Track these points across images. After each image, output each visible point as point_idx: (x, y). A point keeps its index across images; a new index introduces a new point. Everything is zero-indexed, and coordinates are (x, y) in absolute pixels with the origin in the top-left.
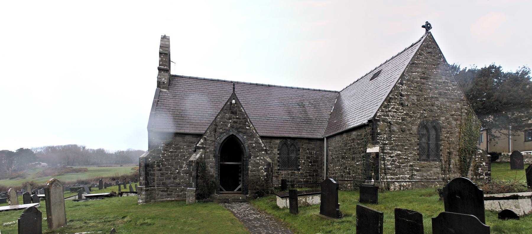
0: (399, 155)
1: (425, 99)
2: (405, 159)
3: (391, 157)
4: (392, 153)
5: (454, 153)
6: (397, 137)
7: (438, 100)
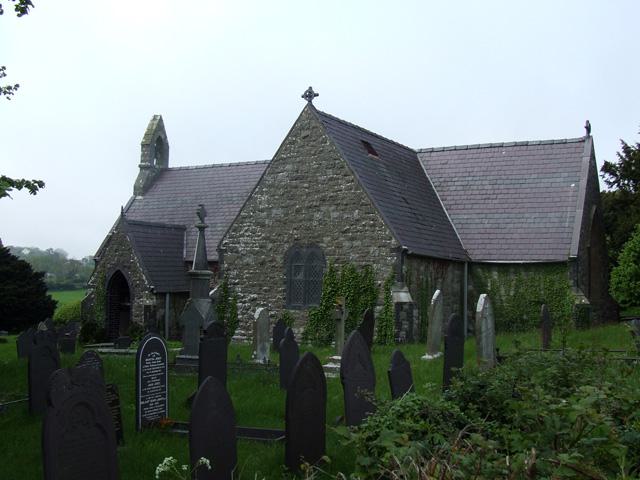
0: (254, 300)
1: (298, 211)
3: (245, 302)
7: (319, 211)
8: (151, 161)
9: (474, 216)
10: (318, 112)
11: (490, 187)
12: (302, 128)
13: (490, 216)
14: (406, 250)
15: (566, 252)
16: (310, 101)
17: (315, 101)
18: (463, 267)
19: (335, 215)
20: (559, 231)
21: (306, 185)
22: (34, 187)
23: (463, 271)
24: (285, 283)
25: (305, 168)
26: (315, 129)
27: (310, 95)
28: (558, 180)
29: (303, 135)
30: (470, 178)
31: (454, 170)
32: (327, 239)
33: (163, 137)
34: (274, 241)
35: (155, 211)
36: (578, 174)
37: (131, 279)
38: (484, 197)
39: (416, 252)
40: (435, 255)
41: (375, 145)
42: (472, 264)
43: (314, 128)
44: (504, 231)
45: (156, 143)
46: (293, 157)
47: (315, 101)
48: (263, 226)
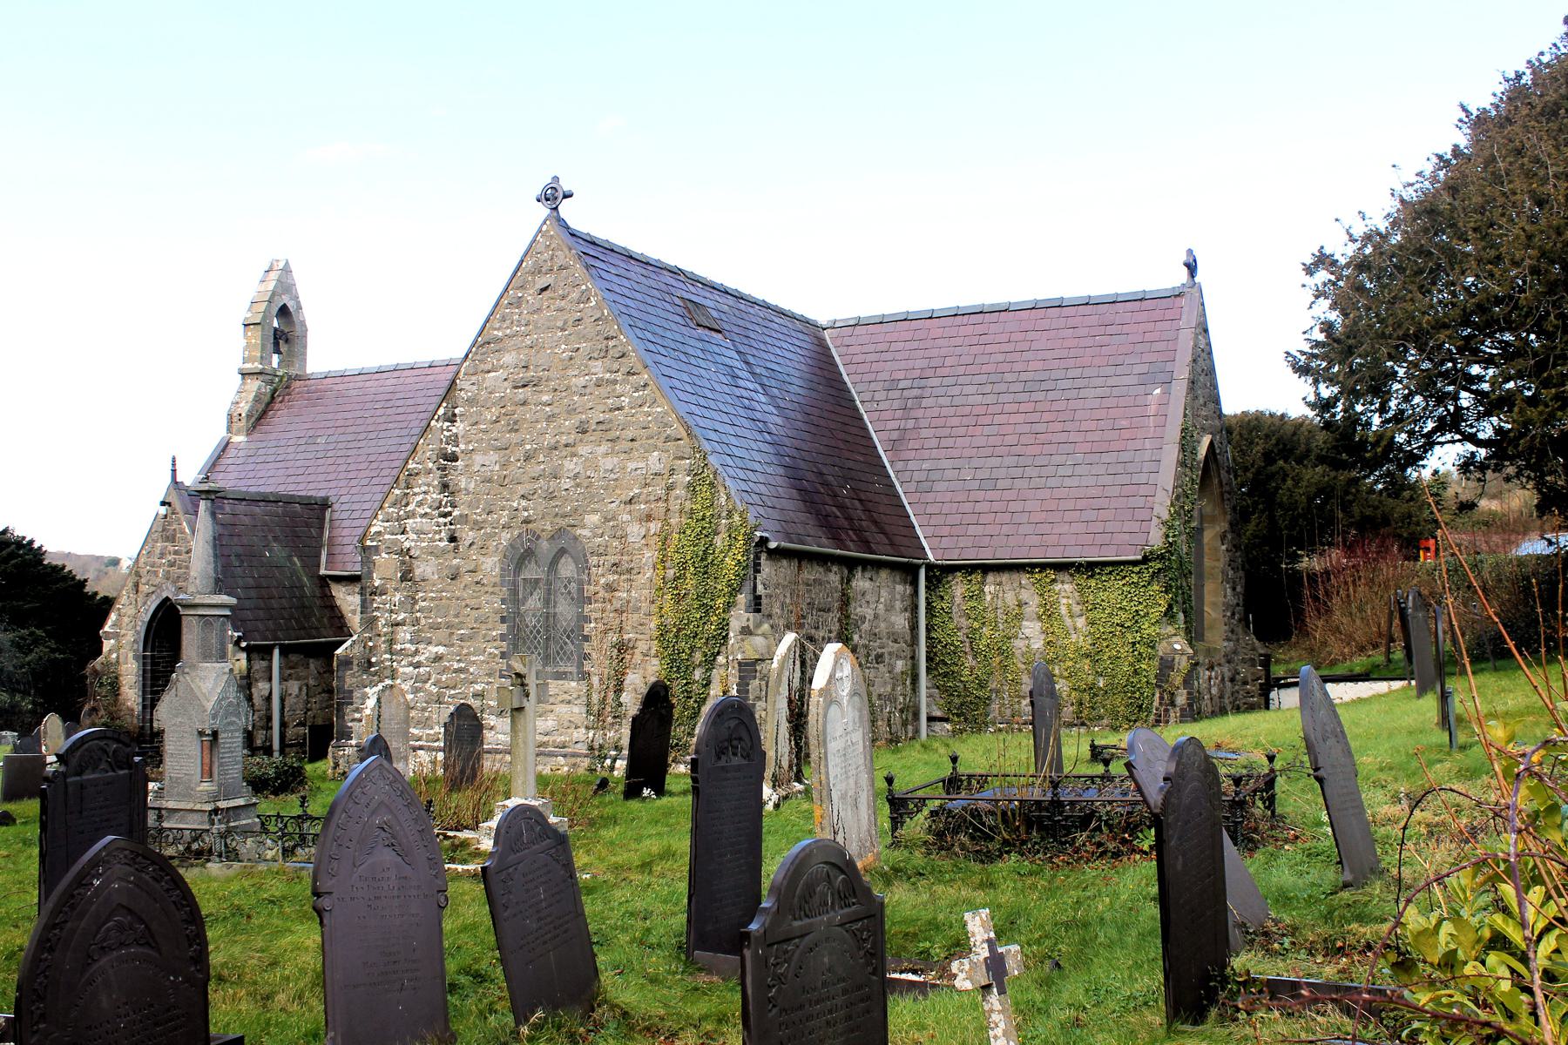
0: (438, 658)
1: (528, 457)
2: (460, 670)
3: (417, 665)
4: (417, 652)
5: (642, 646)
6: (432, 599)
7: (574, 455)
12: (538, 271)
15: (1140, 539)
17: (565, 209)
18: (271, 654)
19: (609, 463)
21: (545, 398)
24: (503, 620)
25: (542, 359)
26: (592, 279)
27: (553, 196)
29: (540, 286)
31: (903, 365)
33: (291, 305)
34: (477, 526)
35: (279, 473)
36: (1169, 367)
43: (561, 268)
44: (1007, 495)
45: (281, 328)
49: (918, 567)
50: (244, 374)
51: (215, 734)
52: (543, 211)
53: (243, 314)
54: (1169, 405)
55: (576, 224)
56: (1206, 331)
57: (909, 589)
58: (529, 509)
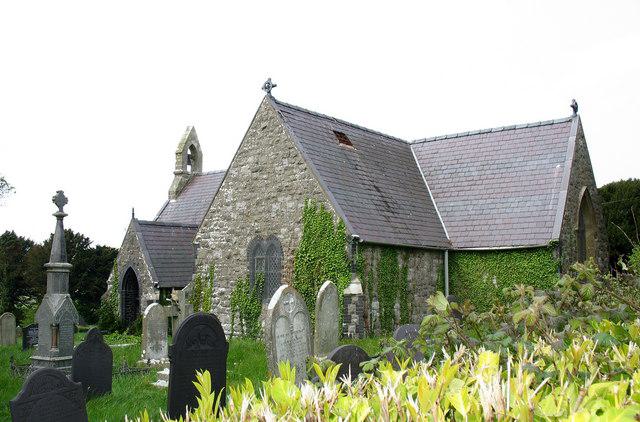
0: (222, 294)
7: (276, 201)
8: (184, 167)
9: (460, 203)
10: (277, 103)
11: (477, 173)
12: (261, 120)
13: (475, 202)
14: (356, 239)
15: (548, 236)
16: (269, 92)
17: (274, 92)
19: (290, 205)
20: (542, 215)
21: (265, 176)
22: (60, 200)
23: (443, 259)
25: (263, 159)
26: (279, 119)
27: (269, 86)
28: (544, 162)
30: (458, 166)
32: (283, 230)
33: (196, 145)
34: (238, 235)
37: (140, 276)
38: (470, 183)
39: (368, 240)
40: (398, 243)
41: (348, 133)
42: (452, 253)
44: (487, 217)
46: (253, 149)
47: (274, 92)
48: (229, 219)
49: (443, 252)
50: (176, 174)
51: (58, 326)
52: (265, 93)
53: (175, 148)
54: (563, 170)
55: (279, 98)
56: (583, 137)
57: (441, 262)
58: (257, 226)
